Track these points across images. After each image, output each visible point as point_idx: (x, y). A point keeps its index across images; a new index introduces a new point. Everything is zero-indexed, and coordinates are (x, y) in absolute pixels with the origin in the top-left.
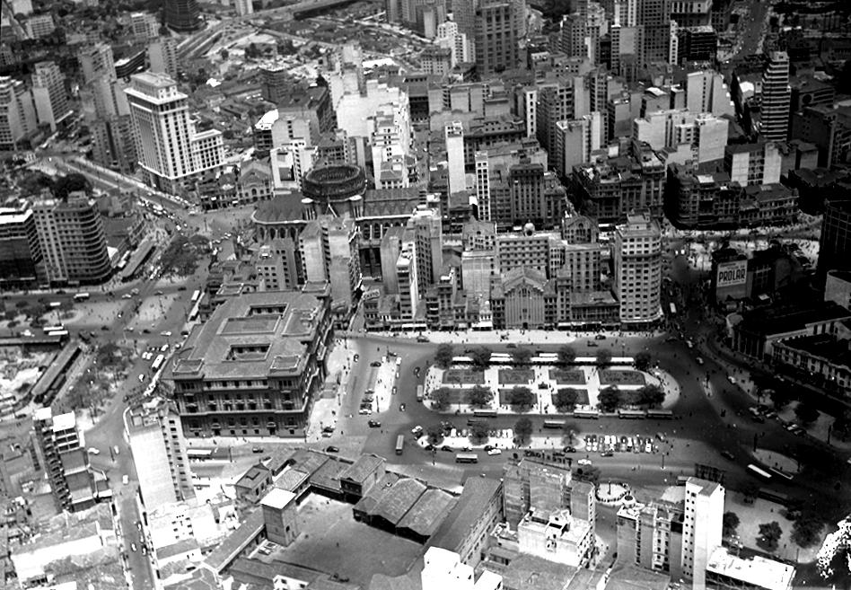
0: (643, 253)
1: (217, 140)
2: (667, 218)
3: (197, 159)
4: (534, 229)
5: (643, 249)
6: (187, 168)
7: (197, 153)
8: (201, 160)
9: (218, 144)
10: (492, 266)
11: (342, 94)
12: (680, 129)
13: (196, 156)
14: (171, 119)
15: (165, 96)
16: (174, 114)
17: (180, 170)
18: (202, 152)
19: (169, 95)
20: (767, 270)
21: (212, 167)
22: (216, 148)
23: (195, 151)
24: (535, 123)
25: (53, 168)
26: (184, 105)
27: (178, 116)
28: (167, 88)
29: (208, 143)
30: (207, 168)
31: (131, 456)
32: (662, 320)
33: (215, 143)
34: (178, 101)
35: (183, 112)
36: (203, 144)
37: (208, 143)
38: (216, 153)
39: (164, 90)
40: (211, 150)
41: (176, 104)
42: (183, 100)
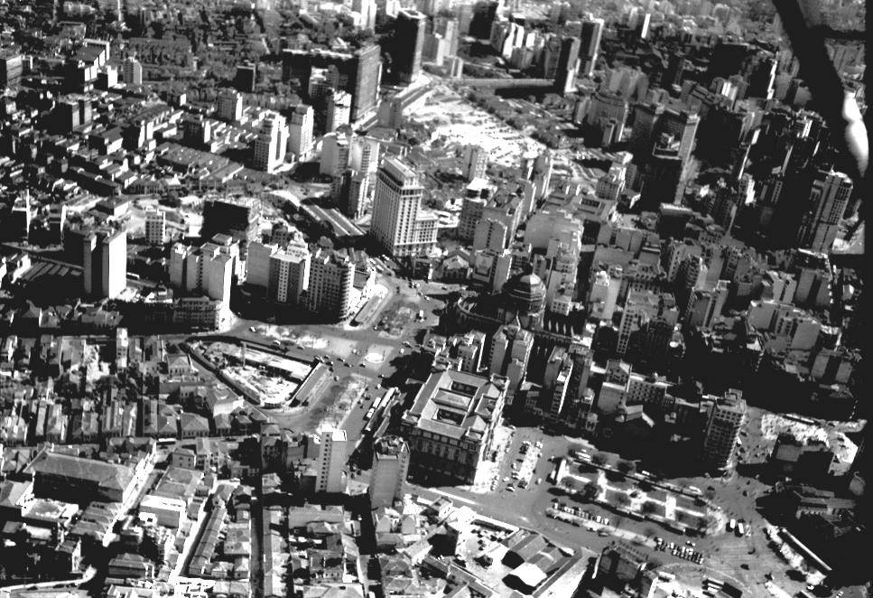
2: (561, 55)
3: (417, 234)
6: (407, 240)
10: (622, 398)
11: (528, 225)
12: (782, 320)
17: (402, 239)
19: (411, 184)
20: (591, 15)
21: (425, 242)
25: (474, 421)
27: (413, 201)
28: (412, 179)
30: (422, 242)
32: (531, 128)
42: (420, 190)
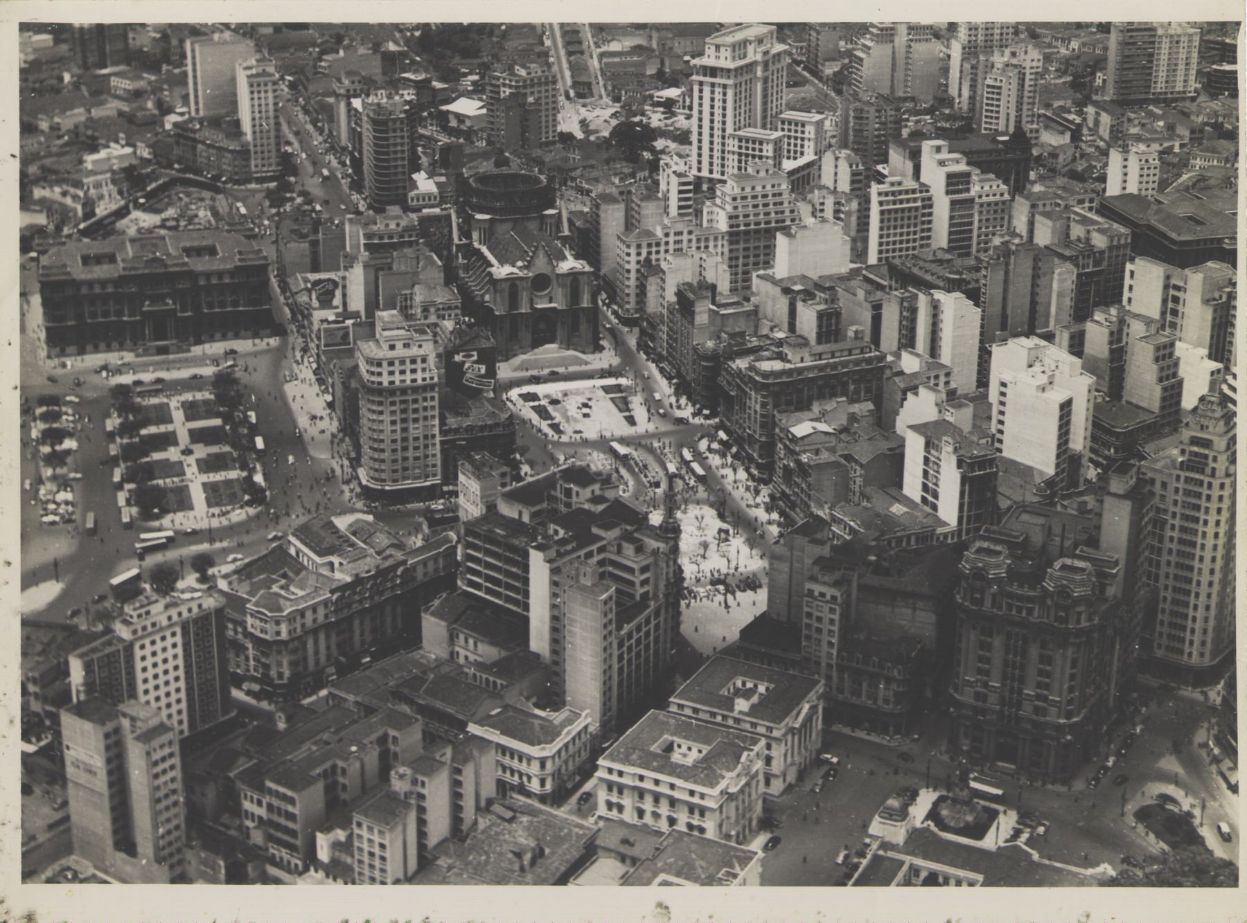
0: (408, 382)
1: (765, 147)
4: (769, 791)
5: (408, 377)
6: (715, 168)
7: (734, 153)
8: (736, 164)
9: (806, 135)
13: (731, 156)
14: (707, 90)
15: (713, 57)
16: (713, 85)
17: (705, 166)
18: (740, 154)
19: (718, 57)
22: (803, 139)
23: (731, 148)
24: (1210, 634)
26: (729, 77)
27: (718, 90)
29: (750, 145)
31: (236, 876)
33: (803, 132)
34: (722, 70)
35: (725, 86)
36: (743, 144)
37: (750, 145)
38: (802, 146)
39: (713, 48)
40: (796, 138)
41: (719, 73)
